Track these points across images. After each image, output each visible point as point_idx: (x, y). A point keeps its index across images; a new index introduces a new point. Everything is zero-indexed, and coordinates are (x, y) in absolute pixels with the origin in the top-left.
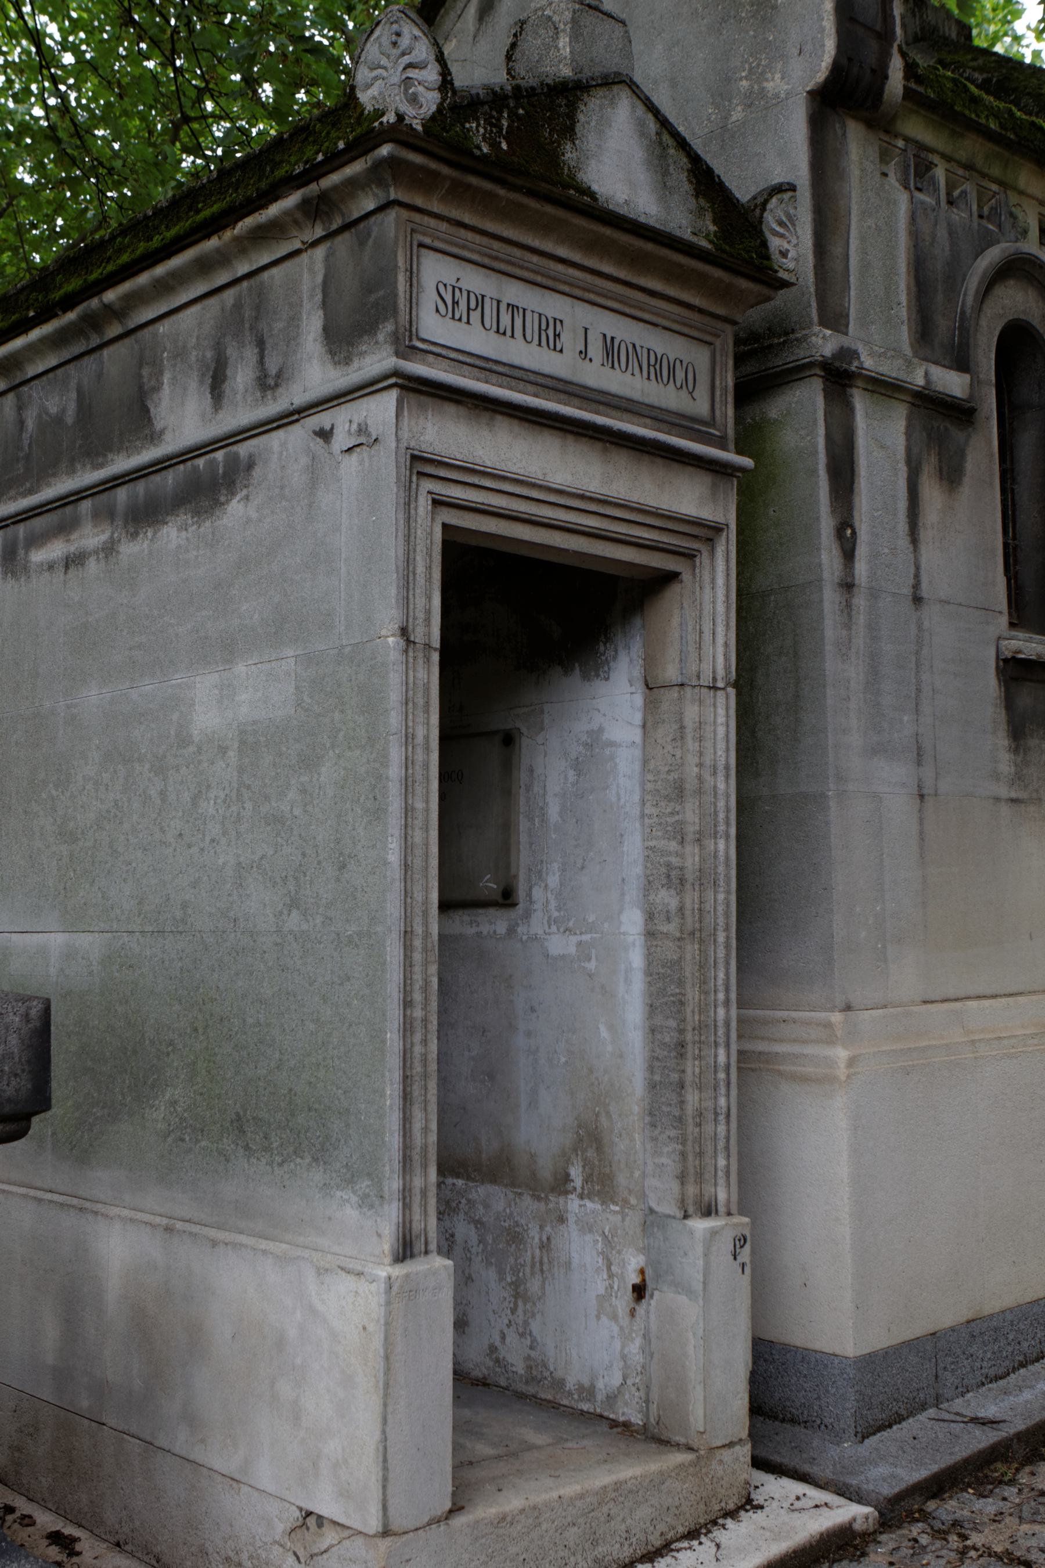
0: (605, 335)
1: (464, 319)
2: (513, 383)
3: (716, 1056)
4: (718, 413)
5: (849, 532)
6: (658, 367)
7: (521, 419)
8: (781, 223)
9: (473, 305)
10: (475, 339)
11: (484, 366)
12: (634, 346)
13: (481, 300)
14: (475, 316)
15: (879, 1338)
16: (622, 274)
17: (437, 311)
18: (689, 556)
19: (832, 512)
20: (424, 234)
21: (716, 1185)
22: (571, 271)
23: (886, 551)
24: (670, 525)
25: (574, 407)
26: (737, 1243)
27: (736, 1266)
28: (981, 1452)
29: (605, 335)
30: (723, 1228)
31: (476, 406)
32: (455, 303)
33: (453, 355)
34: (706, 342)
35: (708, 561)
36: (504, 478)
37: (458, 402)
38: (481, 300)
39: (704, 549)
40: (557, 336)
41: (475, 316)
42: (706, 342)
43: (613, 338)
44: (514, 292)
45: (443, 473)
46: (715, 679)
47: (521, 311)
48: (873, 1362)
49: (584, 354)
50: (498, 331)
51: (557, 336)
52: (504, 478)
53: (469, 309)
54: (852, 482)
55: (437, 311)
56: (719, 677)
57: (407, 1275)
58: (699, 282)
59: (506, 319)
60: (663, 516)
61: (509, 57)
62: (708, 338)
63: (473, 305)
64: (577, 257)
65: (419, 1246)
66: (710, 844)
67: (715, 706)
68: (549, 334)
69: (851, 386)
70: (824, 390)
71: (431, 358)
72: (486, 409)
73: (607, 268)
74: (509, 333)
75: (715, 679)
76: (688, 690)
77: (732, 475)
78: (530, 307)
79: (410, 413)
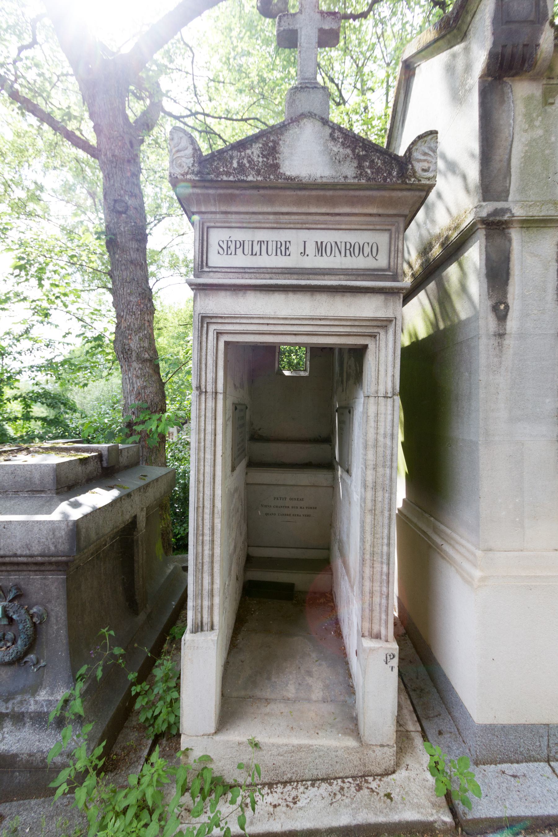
0: (317, 242)
1: (233, 253)
2: (258, 275)
3: (382, 568)
4: (392, 264)
5: (502, 307)
6: (352, 250)
7: (261, 290)
8: (425, 154)
9: (238, 246)
10: (240, 260)
11: (244, 271)
12: (336, 243)
13: (242, 244)
14: (239, 251)
15: (503, 717)
16: (323, 210)
17: (219, 253)
18: (373, 336)
19: (489, 298)
20: (210, 222)
21: (380, 625)
22: (293, 217)
23: (535, 312)
24: (357, 323)
25: (294, 279)
26: (388, 657)
27: (388, 667)
28: (549, 817)
29: (317, 242)
30: (378, 648)
31: (234, 290)
32: (228, 247)
33: (224, 270)
34: (386, 230)
35: (384, 337)
36: (253, 318)
37: (226, 290)
38: (242, 244)
39: (382, 333)
40: (287, 248)
41: (239, 251)
42: (386, 230)
43: (322, 243)
44: (262, 235)
45: (220, 321)
46: (386, 393)
47: (266, 243)
48: (494, 729)
49: (304, 253)
50: (252, 254)
51: (287, 248)
52: (253, 318)
53: (236, 248)
54: (508, 279)
55: (219, 253)
56: (389, 392)
57: (193, 641)
58: (370, 201)
59: (256, 248)
60: (351, 320)
61: (420, 137)
62: (387, 227)
63: (238, 246)
64: (295, 210)
65: (205, 628)
66: (380, 470)
67: (386, 405)
68: (283, 249)
69: (509, 228)
70: (486, 235)
71: (212, 274)
72: (240, 290)
73: (313, 210)
74: (258, 253)
75: (386, 393)
76: (370, 398)
77: (398, 293)
78: (270, 240)
79: (200, 298)
